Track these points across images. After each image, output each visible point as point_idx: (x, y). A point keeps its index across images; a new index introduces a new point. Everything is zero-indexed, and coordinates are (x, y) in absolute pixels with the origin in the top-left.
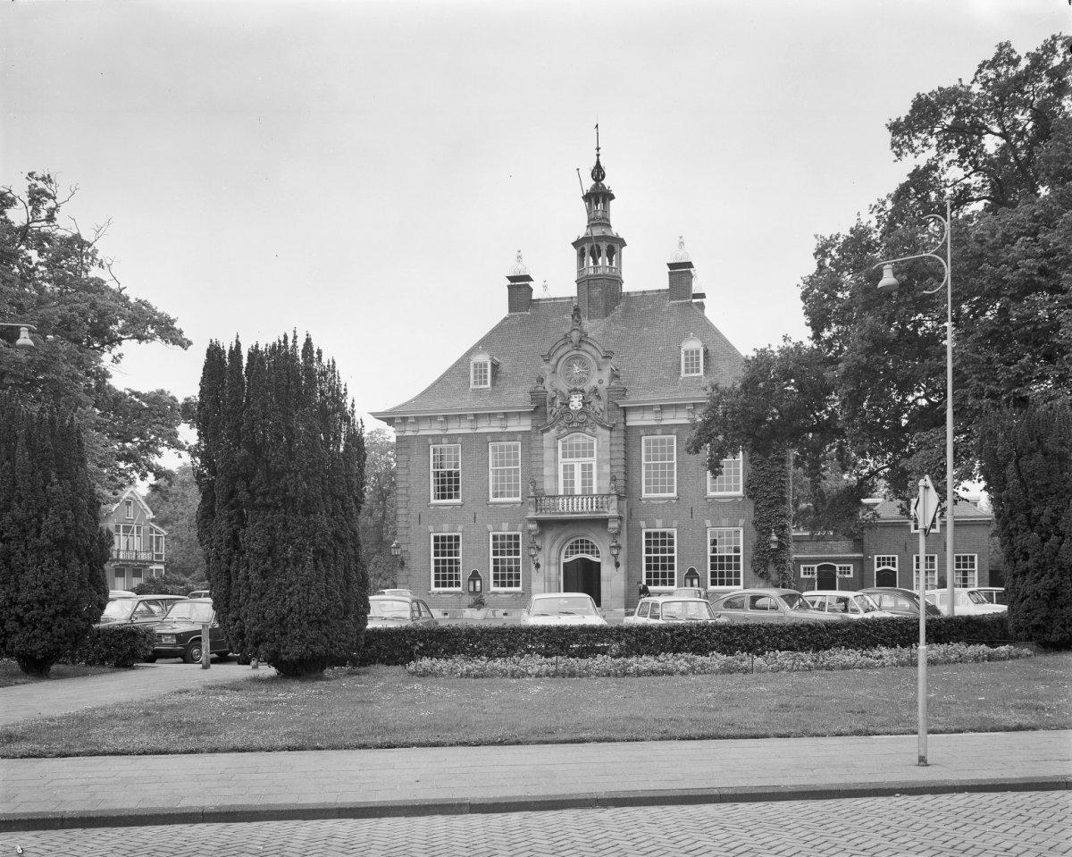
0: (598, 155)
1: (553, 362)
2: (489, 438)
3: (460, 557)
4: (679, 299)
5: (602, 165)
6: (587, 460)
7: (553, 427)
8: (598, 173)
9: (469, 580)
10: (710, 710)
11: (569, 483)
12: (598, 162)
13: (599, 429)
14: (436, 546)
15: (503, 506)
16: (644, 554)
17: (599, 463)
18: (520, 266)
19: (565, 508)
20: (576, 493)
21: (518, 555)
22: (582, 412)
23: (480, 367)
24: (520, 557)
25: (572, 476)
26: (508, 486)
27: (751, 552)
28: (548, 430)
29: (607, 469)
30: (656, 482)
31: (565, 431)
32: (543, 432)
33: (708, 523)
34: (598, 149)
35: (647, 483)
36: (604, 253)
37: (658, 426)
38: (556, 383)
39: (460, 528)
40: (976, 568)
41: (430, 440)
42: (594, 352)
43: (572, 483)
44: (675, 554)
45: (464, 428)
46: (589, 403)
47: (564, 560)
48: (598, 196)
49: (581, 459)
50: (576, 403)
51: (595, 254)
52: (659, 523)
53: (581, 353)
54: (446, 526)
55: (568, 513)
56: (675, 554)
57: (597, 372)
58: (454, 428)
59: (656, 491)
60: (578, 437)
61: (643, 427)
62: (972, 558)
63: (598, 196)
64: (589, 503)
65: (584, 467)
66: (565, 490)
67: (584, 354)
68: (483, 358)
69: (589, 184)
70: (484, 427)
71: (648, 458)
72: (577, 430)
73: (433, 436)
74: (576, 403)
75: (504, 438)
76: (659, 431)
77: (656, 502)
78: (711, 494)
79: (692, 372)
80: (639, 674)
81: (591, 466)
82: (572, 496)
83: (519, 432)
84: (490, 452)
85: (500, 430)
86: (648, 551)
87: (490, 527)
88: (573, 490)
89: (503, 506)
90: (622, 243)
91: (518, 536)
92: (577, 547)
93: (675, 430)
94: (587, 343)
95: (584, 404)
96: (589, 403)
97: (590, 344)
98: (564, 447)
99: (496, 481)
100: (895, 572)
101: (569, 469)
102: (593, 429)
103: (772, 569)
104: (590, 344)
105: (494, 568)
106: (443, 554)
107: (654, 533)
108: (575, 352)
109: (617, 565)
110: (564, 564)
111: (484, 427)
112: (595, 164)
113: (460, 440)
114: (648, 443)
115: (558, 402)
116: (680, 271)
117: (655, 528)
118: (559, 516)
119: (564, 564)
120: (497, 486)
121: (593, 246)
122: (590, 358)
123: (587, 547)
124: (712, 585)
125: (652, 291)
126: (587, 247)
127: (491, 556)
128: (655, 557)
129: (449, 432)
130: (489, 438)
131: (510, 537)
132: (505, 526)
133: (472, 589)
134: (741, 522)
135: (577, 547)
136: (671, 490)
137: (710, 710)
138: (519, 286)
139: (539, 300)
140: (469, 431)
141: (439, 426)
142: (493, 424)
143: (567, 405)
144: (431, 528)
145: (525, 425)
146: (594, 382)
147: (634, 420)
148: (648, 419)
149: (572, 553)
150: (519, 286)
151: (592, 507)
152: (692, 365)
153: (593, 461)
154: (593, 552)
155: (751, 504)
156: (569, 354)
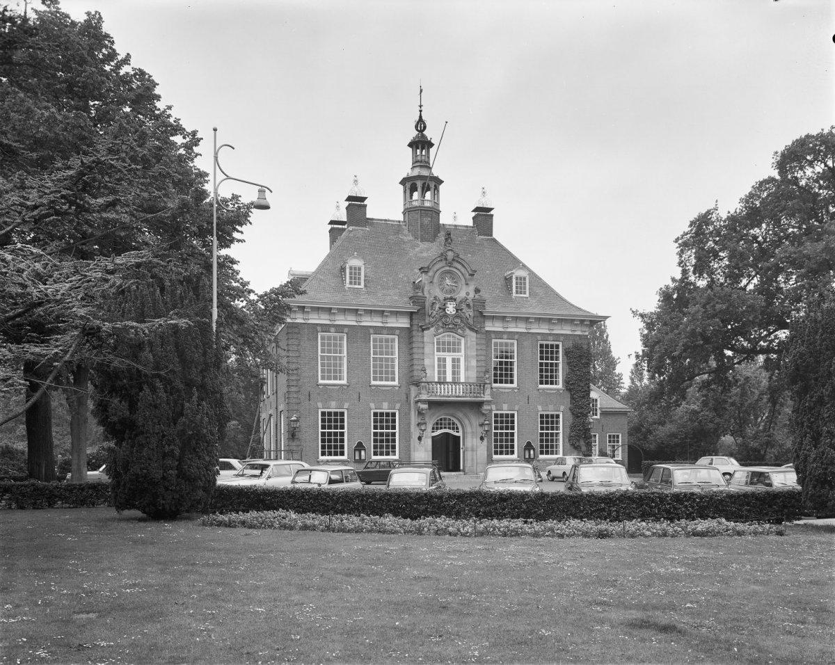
0: (421, 111)
1: (431, 274)
2: (493, 336)
3: (373, 431)
4: (485, 235)
5: (423, 118)
6: (456, 355)
7: (432, 326)
8: (421, 124)
9: (355, 450)
10: (455, 551)
11: (442, 372)
12: (421, 117)
13: (468, 331)
15: (384, 388)
18: (483, 200)
19: (444, 393)
20: (461, 381)
21: (514, 430)
22: (456, 316)
24: (373, 431)
25: (445, 366)
27: (568, 430)
28: (428, 329)
30: (381, 373)
31: (441, 330)
32: (423, 330)
34: (421, 106)
35: (323, 371)
36: (419, 189)
37: (550, 334)
38: (433, 292)
39: (346, 406)
40: (597, 443)
42: (463, 270)
43: (445, 372)
45: (350, 321)
46: (461, 310)
48: (421, 144)
49: (452, 354)
50: (451, 309)
51: (413, 189)
52: (505, 406)
53: (451, 269)
54: (333, 404)
55: (441, 396)
56: (345, 430)
57: (464, 286)
58: (341, 320)
59: (329, 378)
60: (449, 336)
62: (618, 436)
63: (421, 144)
64: (446, 389)
65: (453, 360)
66: (439, 378)
67: (455, 270)
69: (412, 134)
70: (367, 322)
71: (323, 351)
72: (451, 330)
73: (321, 325)
74: (451, 309)
75: (385, 331)
76: (505, 336)
77: (503, 391)
79: (355, 284)
80: (343, 530)
81: (458, 360)
82: (444, 383)
83: (398, 328)
84: (372, 342)
85: (548, 332)
87: (372, 405)
88: (445, 378)
89: (384, 388)
90: (439, 182)
92: (441, 424)
93: (516, 337)
94: (457, 261)
95: (457, 310)
96: (461, 310)
97: (459, 263)
98: (438, 343)
99: (340, 364)
100: (459, 437)
101: (442, 361)
102: (464, 331)
103: (582, 443)
104: (463, 265)
105: (513, 442)
106: (336, 434)
107: (380, 413)
108: (448, 268)
111: (367, 322)
112: (417, 119)
114: (323, 338)
115: (437, 306)
116: (483, 215)
118: (460, 399)
120: (340, 373)
121: (425, 183)
122: (460, 274)
124: (374, 455)
125: (394, 221)
126: (408, 185)
127: (320, 430)
128: (334, 432)
129: (554, 332)
132: (385, 405)
133: (357, 458)
134: (562, 408)
135: (441, 424)
136: (393, 379)
137: (455, 551)
138: (356, 204)
139: (372, 219)
140: (355, 323)
142: (520, 325)
143: (444, 310)
144: (320, 405)
145: (404, 323)
146: (462, 294)
147: (489, 326)
149: (437, 429)
150: (356, 204)
151: (459, 393)
152: (521, 288)
153: (461, 355)
154: (453, 428)
155: (568, 395)
156: (444, 269)
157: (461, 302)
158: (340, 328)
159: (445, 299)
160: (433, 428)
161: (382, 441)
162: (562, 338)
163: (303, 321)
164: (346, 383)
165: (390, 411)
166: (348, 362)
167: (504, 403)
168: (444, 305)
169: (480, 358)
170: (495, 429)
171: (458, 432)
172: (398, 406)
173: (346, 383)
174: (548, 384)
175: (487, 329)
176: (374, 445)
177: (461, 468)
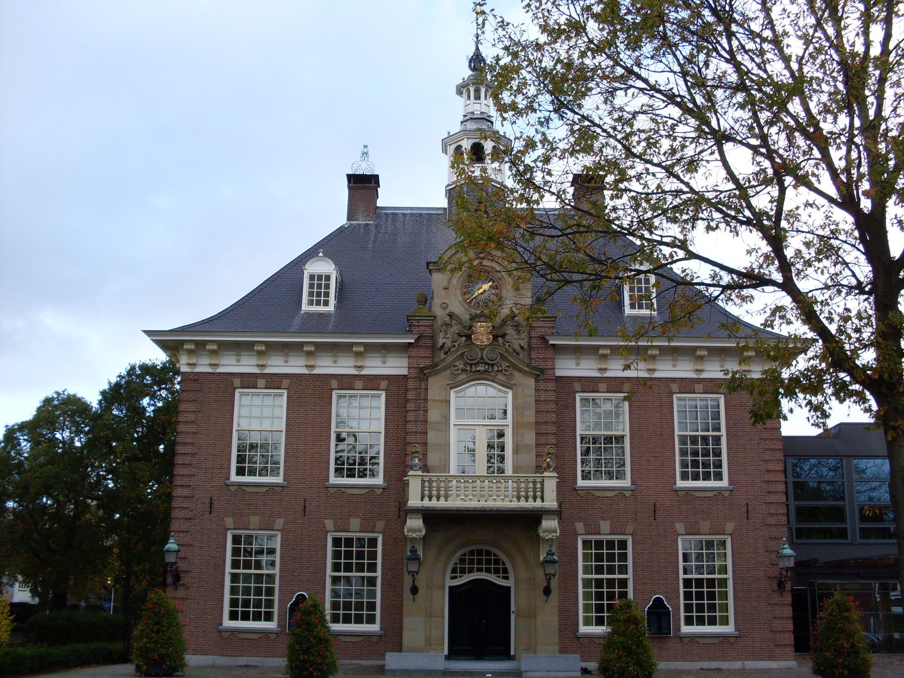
12: (477, 49)
14: (337, 555)
16: (329, 572)
17: (517, 426)
23: (320, 280)
26: (708, 455)
29: (530, 438)
31: (463, 376)
33: (329, 524)
39: (630, 529)
41: (237, 382)
44: (630, 575)
47: (450, 583)
50: (482, 332)
52: (605, 526)
61: (579, 379)
68: (324, 267)
73: (242, 375)
74: (482, 332)
76: (602, 387)
78: (680, 484)
86: (235, 564)
89: (248, 489)
91: (376, 540)
92: (471, 562)
95: (495, 337)
96: (503, 336)
100: (509, 588)
109: (547, 591)
110: (451, 588)
113: (286, 382)
117: (599, 534)
119: (451, 588)
123: (488, 562)
128: (596, 580)
130: (334, 384)
131: (610, 544)
132: (355, 523)
141: (253, 361)
144: (229, 522)
147: (567, 368)
148: (586, 368)
149: (463, 571)
154: (496, 571)
157: (504, 322)
158: (615, 385)
159: (473, 318)
160: (454, 571)
161: (700, 596)
162: (384, 384)
163: (209, 370)
164: (629, 485)
165: (367, 535)
166: (728, 440)
167: (603, 519)
168: (470, 328)
169: (543, 428)
170: (584, 573)
171: (507, 578)
172: (380, 525)
173: (629, 485)
174: (709, 479)
175: (559, 373)
176: (685, 605)
177: (512, 653)
